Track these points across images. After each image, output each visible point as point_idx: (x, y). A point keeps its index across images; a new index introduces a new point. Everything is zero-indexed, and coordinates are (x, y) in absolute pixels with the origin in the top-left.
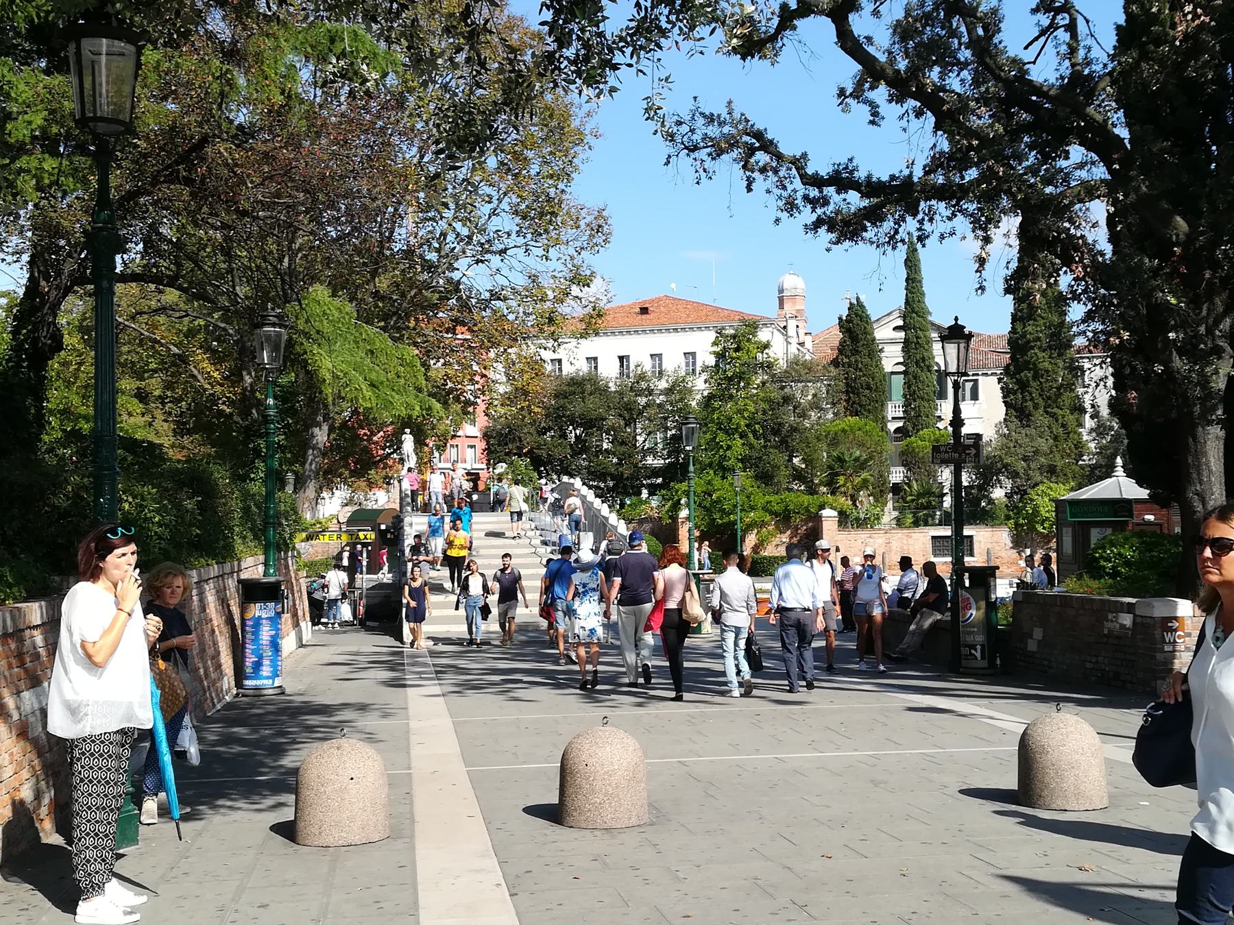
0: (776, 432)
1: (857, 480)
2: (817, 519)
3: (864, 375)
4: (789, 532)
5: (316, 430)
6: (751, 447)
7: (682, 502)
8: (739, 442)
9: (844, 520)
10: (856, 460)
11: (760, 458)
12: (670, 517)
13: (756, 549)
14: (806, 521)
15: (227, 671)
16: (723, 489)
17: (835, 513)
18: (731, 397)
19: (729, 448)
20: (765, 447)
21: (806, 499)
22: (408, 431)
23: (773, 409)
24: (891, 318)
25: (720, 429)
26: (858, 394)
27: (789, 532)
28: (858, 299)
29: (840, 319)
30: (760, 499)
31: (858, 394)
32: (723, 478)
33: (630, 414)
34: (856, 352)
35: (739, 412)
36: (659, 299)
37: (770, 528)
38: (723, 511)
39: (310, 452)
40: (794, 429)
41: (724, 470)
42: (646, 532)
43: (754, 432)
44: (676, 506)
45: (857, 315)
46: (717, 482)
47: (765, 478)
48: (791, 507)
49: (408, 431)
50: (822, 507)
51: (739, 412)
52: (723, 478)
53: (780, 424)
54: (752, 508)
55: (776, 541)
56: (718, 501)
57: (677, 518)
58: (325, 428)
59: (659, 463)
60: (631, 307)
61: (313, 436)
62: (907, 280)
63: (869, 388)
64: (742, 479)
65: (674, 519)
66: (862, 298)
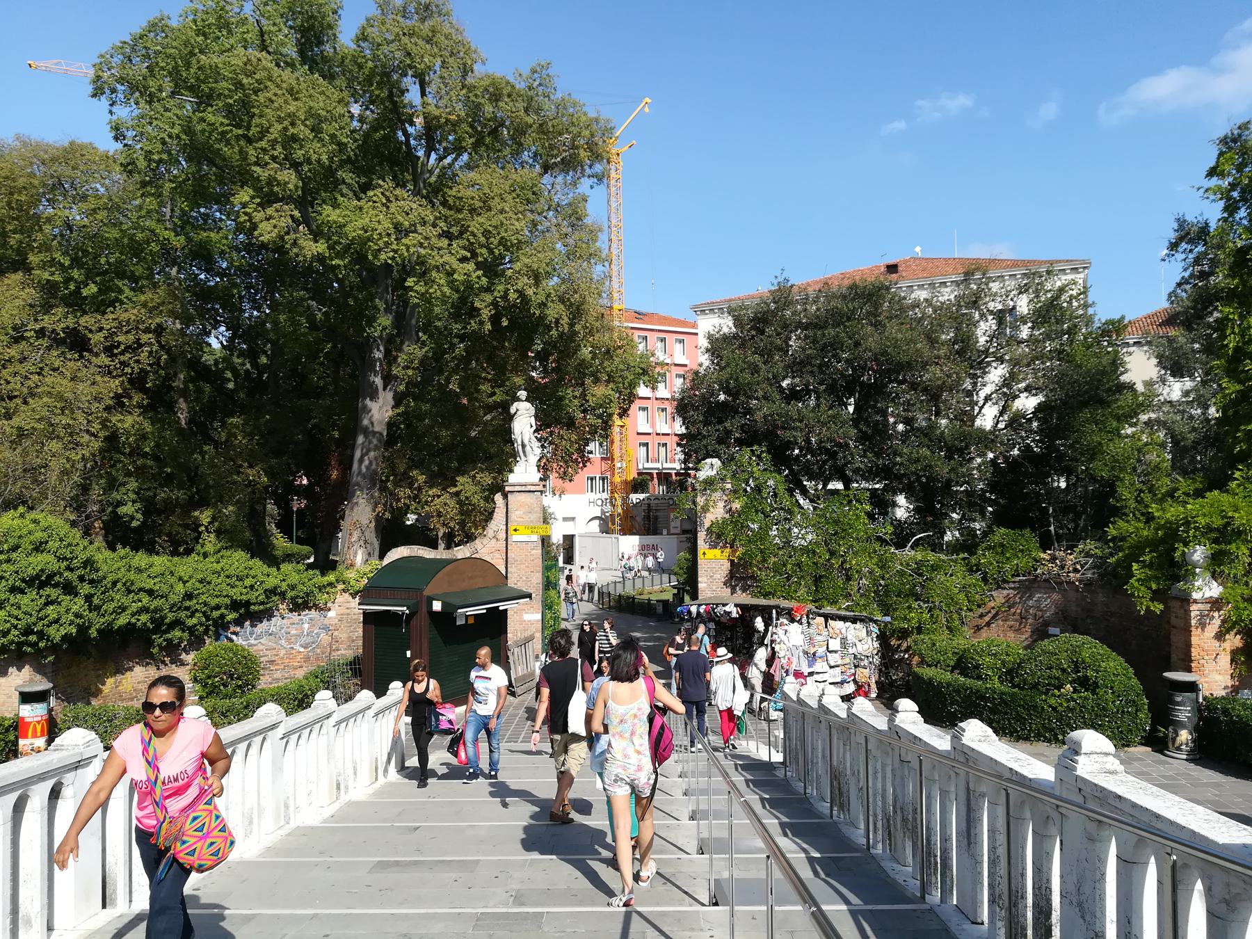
57: (1186, 600)
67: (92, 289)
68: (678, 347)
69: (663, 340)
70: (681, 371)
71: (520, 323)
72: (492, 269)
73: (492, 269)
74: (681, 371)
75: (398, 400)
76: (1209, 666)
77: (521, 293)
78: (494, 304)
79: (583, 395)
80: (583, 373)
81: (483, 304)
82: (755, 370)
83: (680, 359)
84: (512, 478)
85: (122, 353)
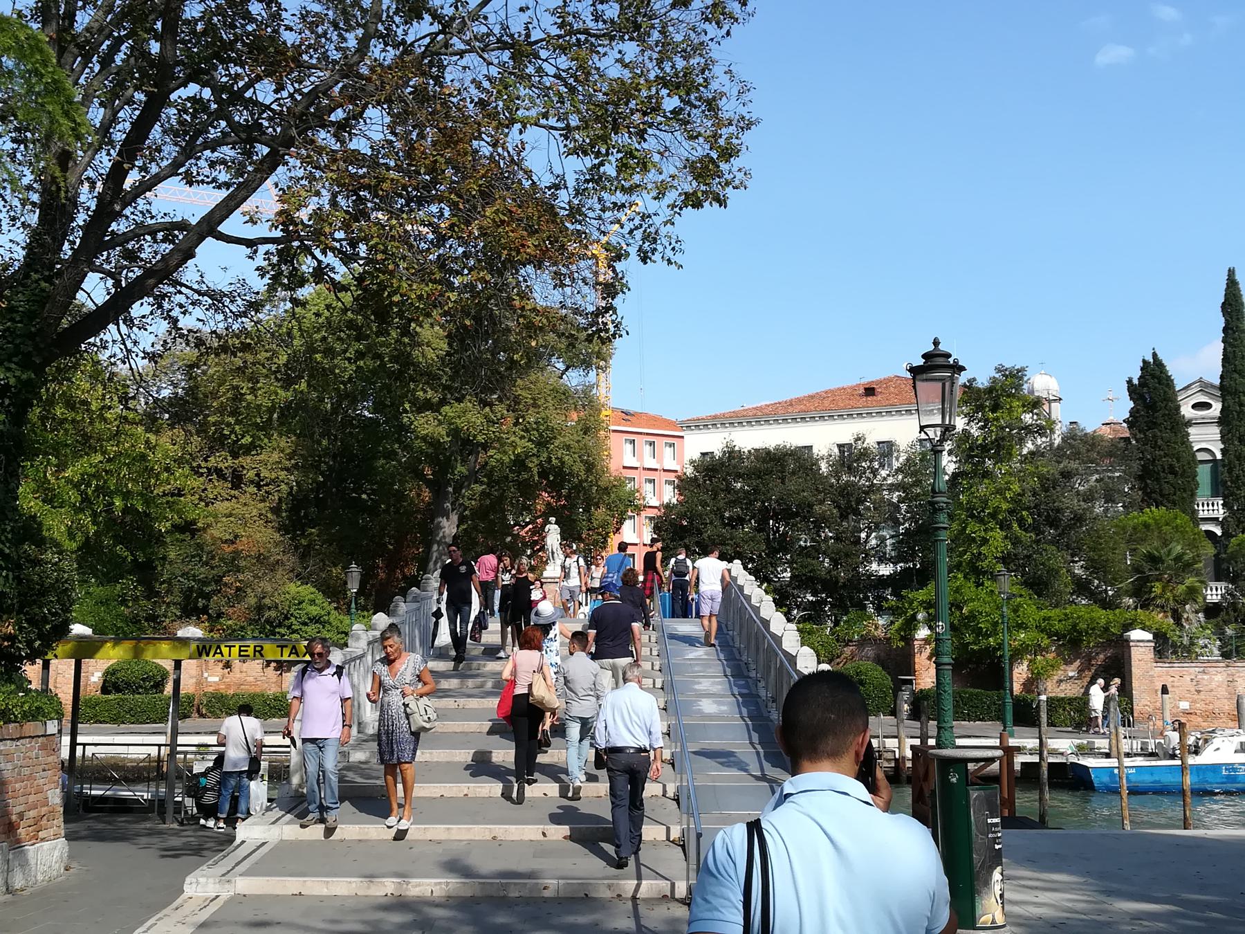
0: (1053, 522)
1: (1181, 588)
2: (1123, 645)
3: (1166, 455)
4: (1077, 663)
5: (444, 522)
6: (1016, 542)
7: (920, 616)
8: (998, 534)
9: (1164, 647)
10: (1178, 558)
11: (1029, 557)
12: (902, 638)
13: (1030, 685)
14: (1103, 647)
15: (906, 707)
16: (977, 600)
17: (1150, 636)
18: (986, 474)
19: (985, 541)
20: (1038, 542)
21: (1102, 616)
22: (553, 519)
23: (1046, 490)
24: (1190, 392)
25: (972, 516)
26: (1158, 480)
27: (1077, 663)
28: (1155, 355)
29: (1130, 382)
30: (1032, 611)
31: (1158, 480)
32: (979, 584)
33: (849, 502)
34: (1152, 425)
35: (1000, 491)
36: (889, 380)
37: (1050, 656)
38: (978, 632)
39: (435, 547)
40: (1078, 519)
41: (976, 572)
42: (868, 658)
43: (1021, 522)
44: (911, 624)
45: (1153, 376)
46: (969, 589)
47: (1038, 585)
48: (1083, 626)
49: (553, 519)
50: (1128, 627)
51: (1000, 491)
52: (979, 584)
53: (1058, 510)
54: (1021, 626)
55: (1059, 674)
56: (972, 616)
57: (913, 639)
58: (454, 518)
59: (886, 570)
60: (853, 388)
61: (439, 527)
62: (1225, 330)
63: (1172, 471)
64: (1007, 583)
65: (908, 640)
66: (1160, 356)
67: (247, 440)
68: (669, 450)
69: (652, 444)
70: (672, 477)
71: (555, 477)
72: (542, 443)
73: (542, 443)
74: (672, 477)
75: (462, 520)
76: (924, 674)
77: (560, 459)
78: (540, 464)
79: (589, 520)
80: (590, 504)
81: (533, 464)
82: (705, 504)
83: (670, 464)
84: (546, 574)
85: (267, 485)
